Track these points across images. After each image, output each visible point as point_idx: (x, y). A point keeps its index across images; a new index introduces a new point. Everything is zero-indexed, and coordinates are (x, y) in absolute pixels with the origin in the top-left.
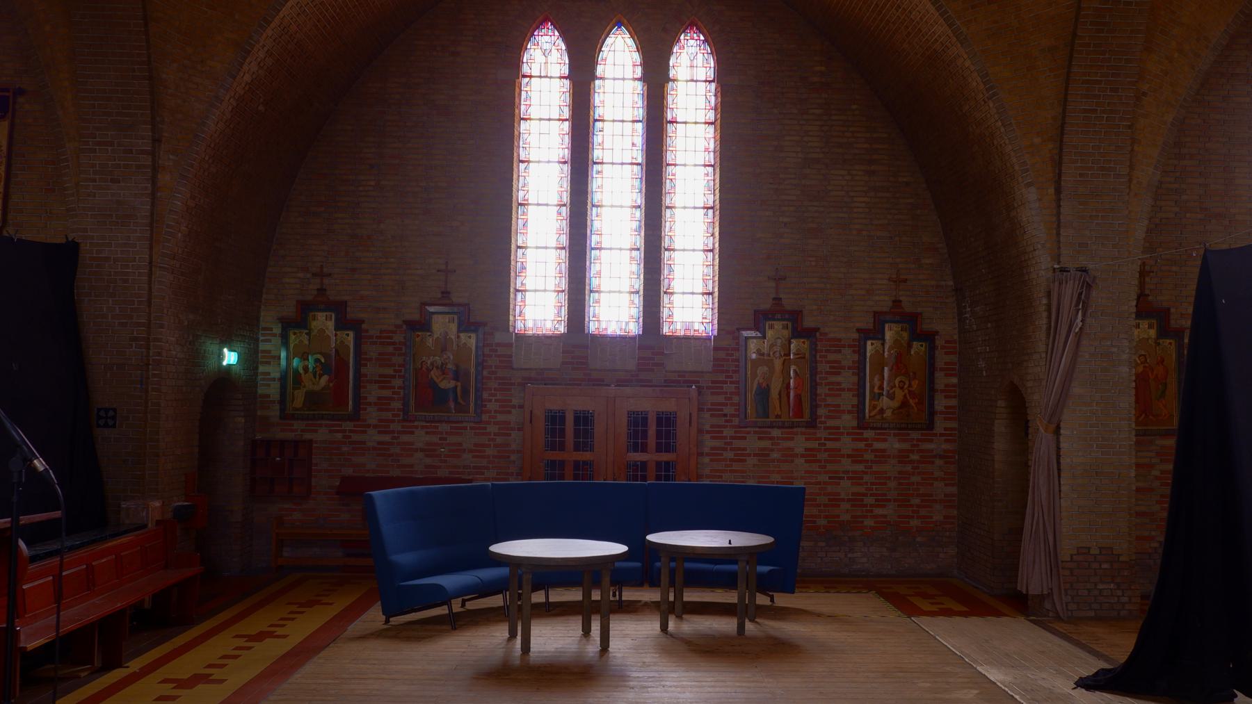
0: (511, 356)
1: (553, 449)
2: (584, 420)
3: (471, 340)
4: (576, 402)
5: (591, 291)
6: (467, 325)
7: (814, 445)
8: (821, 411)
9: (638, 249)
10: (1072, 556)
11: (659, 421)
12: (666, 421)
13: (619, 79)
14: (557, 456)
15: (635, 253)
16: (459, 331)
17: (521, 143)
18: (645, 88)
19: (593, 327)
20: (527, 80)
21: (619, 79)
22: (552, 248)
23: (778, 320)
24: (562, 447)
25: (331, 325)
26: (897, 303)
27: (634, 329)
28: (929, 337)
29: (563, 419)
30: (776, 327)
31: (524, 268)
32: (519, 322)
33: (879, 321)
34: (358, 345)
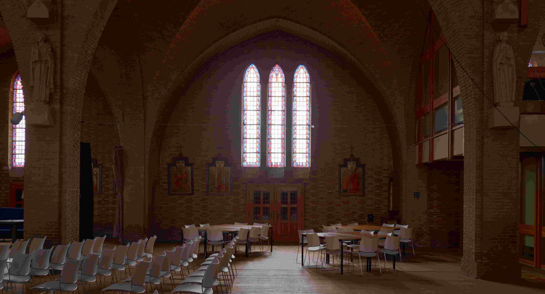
0: (8, 174)
1: (256, 203)
2: (267, 196)
3: (189, 169)
4: (263, 189)
5: (293, 153)
6: (227, 164)
7: (101, 199)
8: (103, 189)
9: (259, 139)
10: (127, 227)
11: (291, 194)
12: (294, 195)
13: (302, 83)
14: (258, 205)
15: (258, 140)
16: (225, 166)
17: (14, 109)
18: (311, 86)
19: (295, 165)
20: (15, 90)
21: (302, 83)
22: (305, 139)
23: (351, 161)
24: (259, 203)
25: (183, 164)
26: (352, 155)
27: (258, 165)
28: (363, 166)
29: (287, 195)
30: (183, 164)
31: (15, 147)
32: (14, 163)
33: (346, 161)
34: (192, 172)
